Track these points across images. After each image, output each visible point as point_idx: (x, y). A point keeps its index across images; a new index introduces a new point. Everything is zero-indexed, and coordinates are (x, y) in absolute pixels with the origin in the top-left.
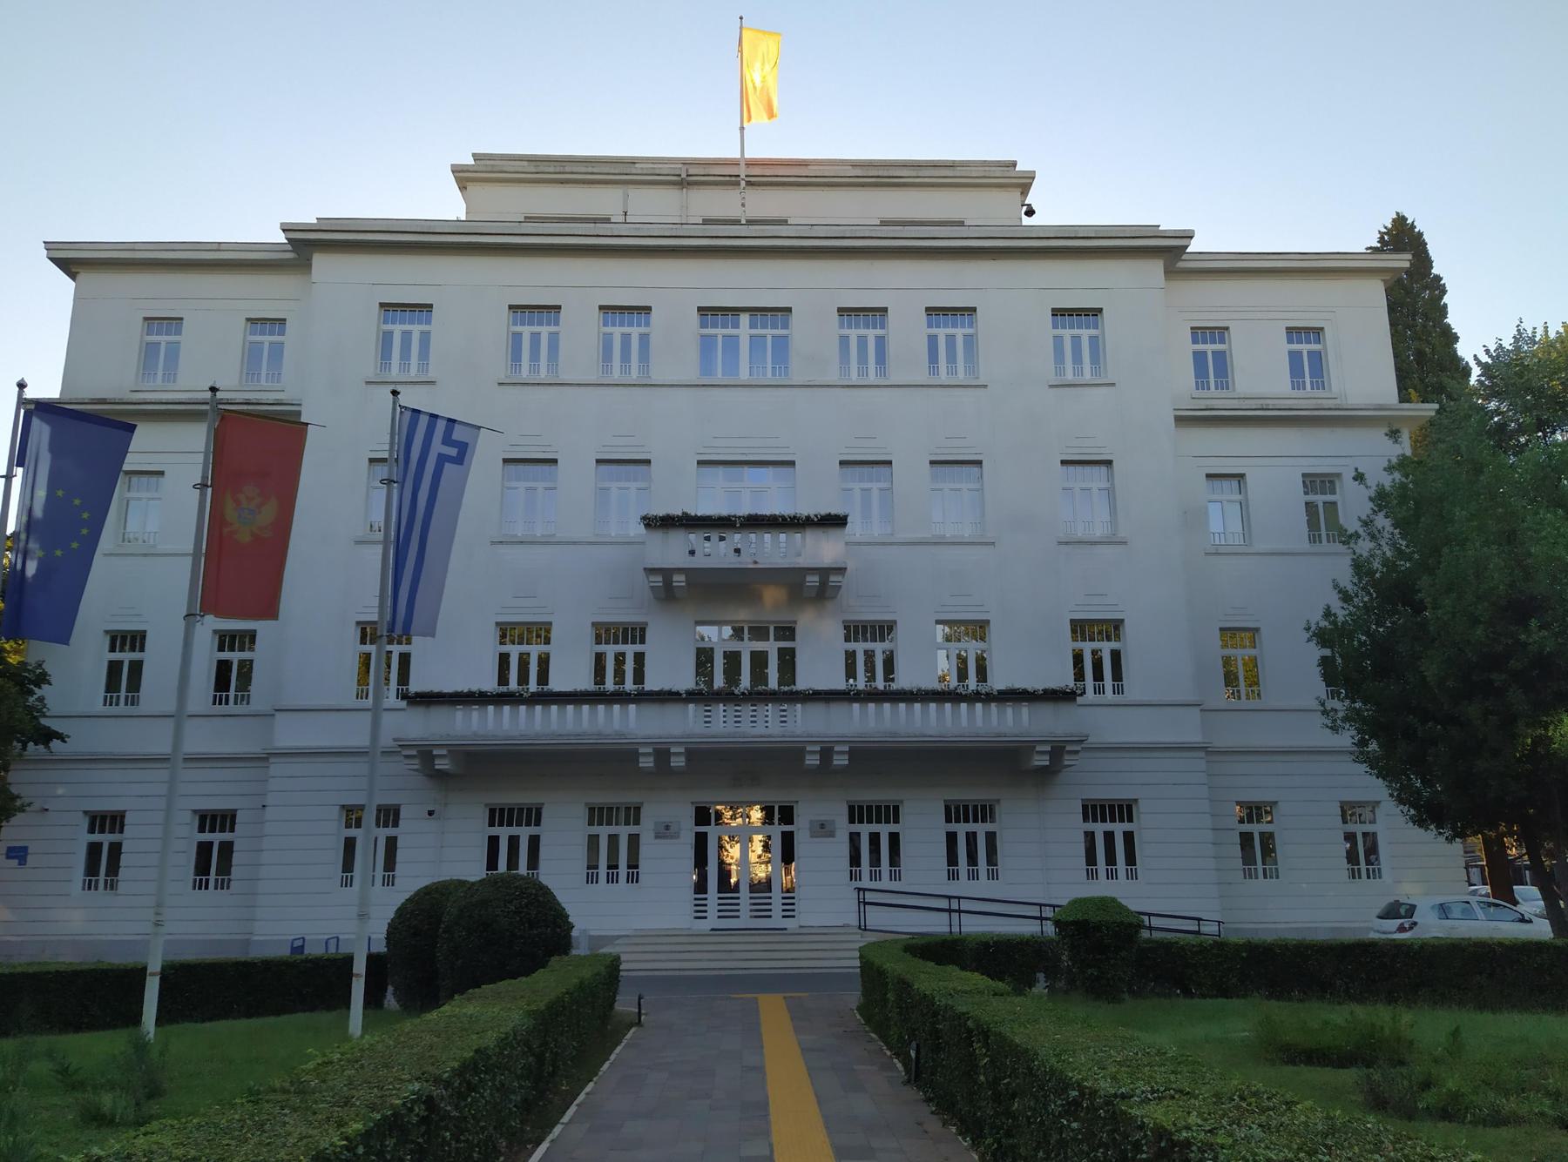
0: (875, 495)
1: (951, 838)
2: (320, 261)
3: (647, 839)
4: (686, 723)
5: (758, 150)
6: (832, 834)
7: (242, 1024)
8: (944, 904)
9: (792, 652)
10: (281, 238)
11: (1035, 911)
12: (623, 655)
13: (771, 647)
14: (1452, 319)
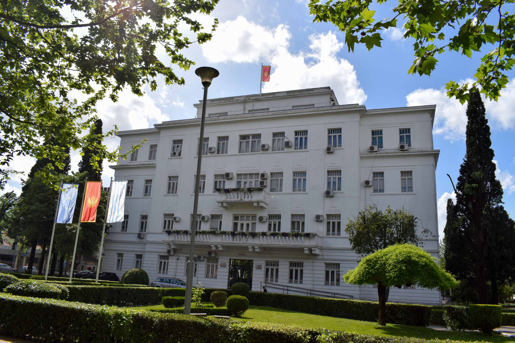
0: (337, 137)
1: (291, 271)
2: (163, 133)
3: (219, 267)
4: (228, 240)
5: (265, 91)
6: (261, 269)
7: (366, 323)
8: (282, 287)
9: (382, 137)
10: (154, 127)
11: (306, 291)
12: (302, 138)
13: (250, 223)
14: (467, 117)
